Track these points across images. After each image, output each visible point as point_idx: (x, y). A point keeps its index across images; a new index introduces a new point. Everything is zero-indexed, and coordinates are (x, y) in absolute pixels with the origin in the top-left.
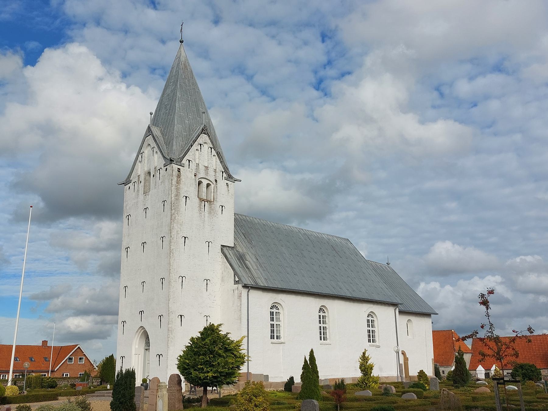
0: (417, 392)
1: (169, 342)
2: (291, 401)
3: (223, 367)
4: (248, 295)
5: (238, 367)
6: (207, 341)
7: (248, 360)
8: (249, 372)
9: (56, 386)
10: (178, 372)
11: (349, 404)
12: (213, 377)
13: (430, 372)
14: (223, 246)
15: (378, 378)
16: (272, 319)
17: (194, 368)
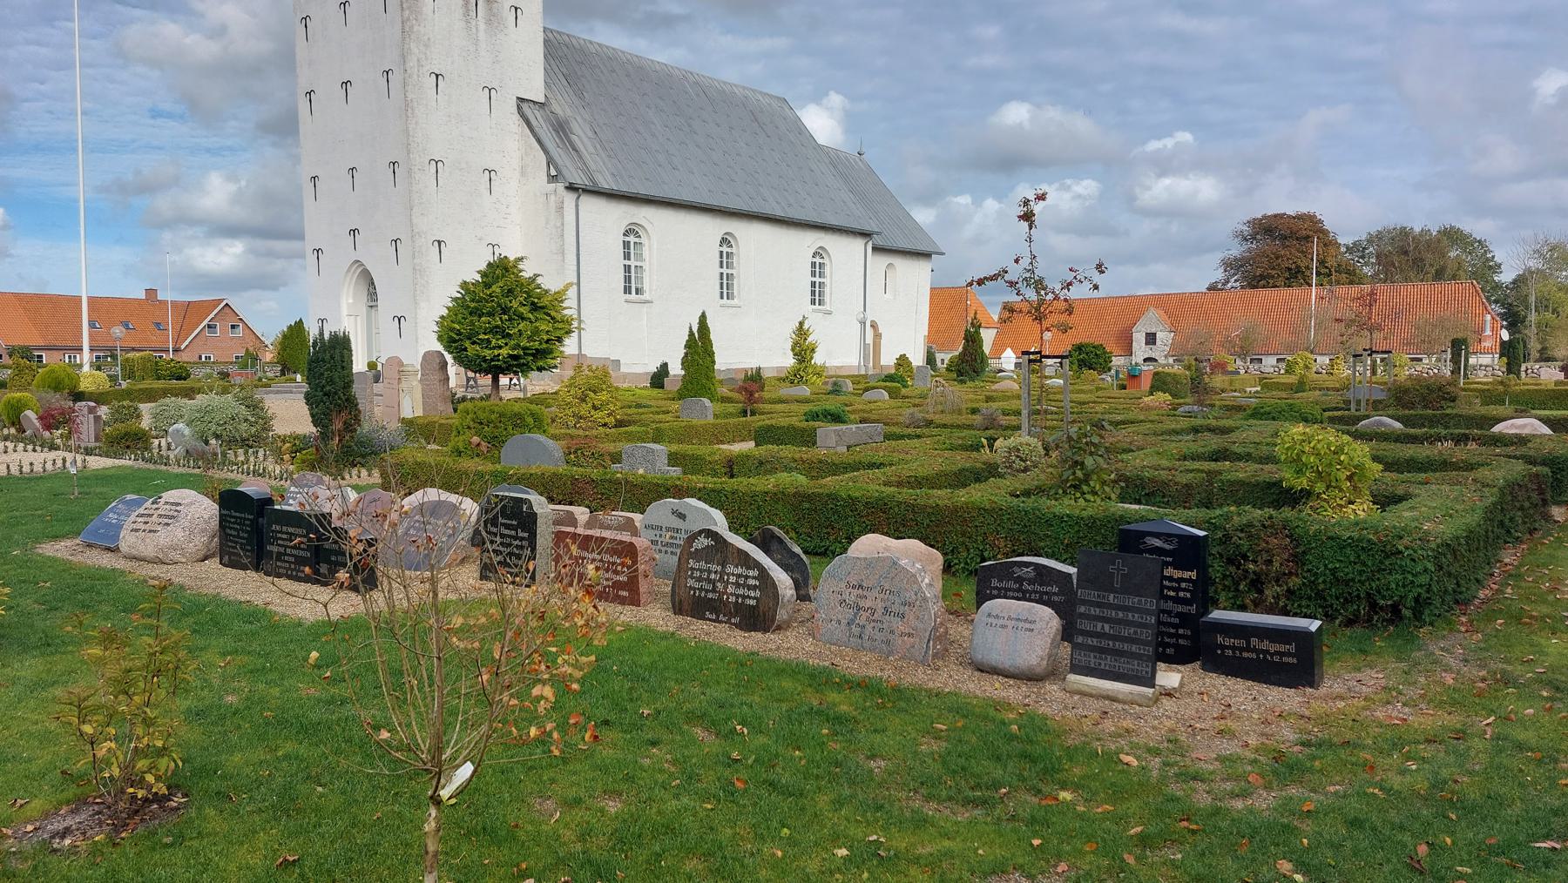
0: (890, 388)
1: (418, 292)
2: (661, 403)
3: (530, 339)
4: (577, 206)
5: (560, 340)
6: (496, 289)
7: (579, 329)
8: (583, 353)
9: (188, 376)
10: (439, 347)
11: (768, 407)
12: (510, 356)
13: (917, 359)
14: (521, 100)
15: (824, 367)
16: (627, 256)
17: (470, 339)
